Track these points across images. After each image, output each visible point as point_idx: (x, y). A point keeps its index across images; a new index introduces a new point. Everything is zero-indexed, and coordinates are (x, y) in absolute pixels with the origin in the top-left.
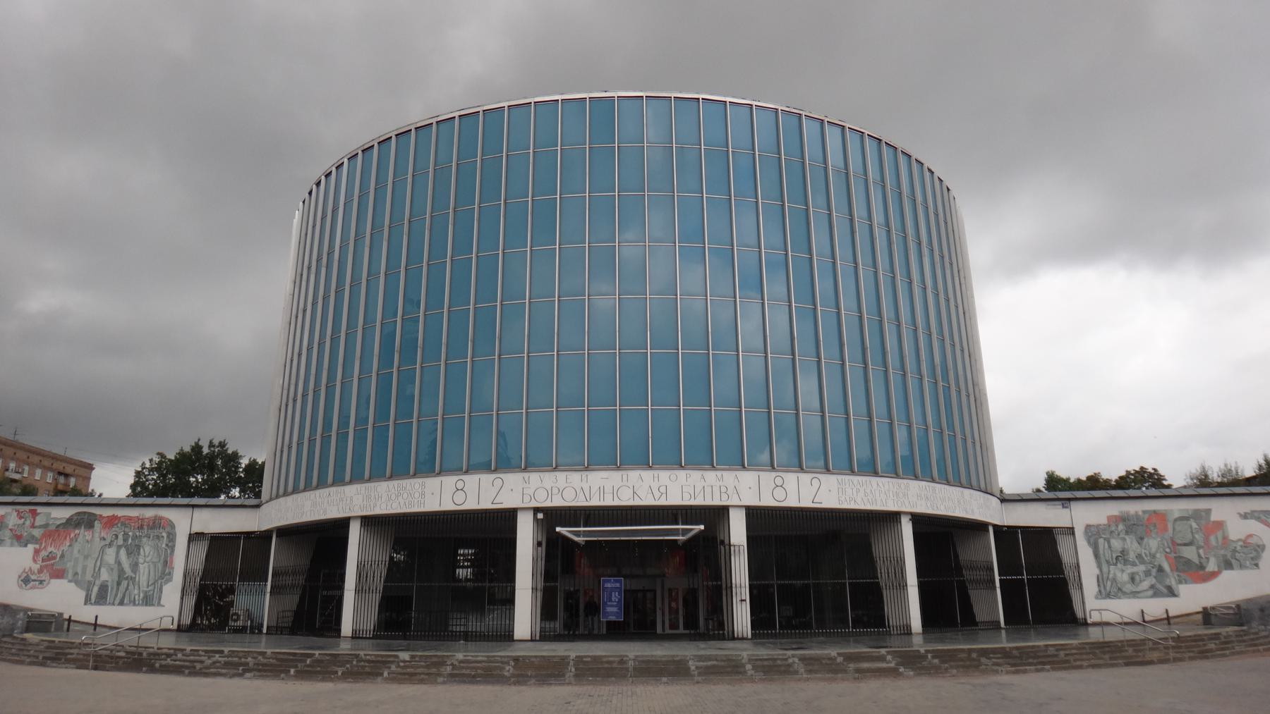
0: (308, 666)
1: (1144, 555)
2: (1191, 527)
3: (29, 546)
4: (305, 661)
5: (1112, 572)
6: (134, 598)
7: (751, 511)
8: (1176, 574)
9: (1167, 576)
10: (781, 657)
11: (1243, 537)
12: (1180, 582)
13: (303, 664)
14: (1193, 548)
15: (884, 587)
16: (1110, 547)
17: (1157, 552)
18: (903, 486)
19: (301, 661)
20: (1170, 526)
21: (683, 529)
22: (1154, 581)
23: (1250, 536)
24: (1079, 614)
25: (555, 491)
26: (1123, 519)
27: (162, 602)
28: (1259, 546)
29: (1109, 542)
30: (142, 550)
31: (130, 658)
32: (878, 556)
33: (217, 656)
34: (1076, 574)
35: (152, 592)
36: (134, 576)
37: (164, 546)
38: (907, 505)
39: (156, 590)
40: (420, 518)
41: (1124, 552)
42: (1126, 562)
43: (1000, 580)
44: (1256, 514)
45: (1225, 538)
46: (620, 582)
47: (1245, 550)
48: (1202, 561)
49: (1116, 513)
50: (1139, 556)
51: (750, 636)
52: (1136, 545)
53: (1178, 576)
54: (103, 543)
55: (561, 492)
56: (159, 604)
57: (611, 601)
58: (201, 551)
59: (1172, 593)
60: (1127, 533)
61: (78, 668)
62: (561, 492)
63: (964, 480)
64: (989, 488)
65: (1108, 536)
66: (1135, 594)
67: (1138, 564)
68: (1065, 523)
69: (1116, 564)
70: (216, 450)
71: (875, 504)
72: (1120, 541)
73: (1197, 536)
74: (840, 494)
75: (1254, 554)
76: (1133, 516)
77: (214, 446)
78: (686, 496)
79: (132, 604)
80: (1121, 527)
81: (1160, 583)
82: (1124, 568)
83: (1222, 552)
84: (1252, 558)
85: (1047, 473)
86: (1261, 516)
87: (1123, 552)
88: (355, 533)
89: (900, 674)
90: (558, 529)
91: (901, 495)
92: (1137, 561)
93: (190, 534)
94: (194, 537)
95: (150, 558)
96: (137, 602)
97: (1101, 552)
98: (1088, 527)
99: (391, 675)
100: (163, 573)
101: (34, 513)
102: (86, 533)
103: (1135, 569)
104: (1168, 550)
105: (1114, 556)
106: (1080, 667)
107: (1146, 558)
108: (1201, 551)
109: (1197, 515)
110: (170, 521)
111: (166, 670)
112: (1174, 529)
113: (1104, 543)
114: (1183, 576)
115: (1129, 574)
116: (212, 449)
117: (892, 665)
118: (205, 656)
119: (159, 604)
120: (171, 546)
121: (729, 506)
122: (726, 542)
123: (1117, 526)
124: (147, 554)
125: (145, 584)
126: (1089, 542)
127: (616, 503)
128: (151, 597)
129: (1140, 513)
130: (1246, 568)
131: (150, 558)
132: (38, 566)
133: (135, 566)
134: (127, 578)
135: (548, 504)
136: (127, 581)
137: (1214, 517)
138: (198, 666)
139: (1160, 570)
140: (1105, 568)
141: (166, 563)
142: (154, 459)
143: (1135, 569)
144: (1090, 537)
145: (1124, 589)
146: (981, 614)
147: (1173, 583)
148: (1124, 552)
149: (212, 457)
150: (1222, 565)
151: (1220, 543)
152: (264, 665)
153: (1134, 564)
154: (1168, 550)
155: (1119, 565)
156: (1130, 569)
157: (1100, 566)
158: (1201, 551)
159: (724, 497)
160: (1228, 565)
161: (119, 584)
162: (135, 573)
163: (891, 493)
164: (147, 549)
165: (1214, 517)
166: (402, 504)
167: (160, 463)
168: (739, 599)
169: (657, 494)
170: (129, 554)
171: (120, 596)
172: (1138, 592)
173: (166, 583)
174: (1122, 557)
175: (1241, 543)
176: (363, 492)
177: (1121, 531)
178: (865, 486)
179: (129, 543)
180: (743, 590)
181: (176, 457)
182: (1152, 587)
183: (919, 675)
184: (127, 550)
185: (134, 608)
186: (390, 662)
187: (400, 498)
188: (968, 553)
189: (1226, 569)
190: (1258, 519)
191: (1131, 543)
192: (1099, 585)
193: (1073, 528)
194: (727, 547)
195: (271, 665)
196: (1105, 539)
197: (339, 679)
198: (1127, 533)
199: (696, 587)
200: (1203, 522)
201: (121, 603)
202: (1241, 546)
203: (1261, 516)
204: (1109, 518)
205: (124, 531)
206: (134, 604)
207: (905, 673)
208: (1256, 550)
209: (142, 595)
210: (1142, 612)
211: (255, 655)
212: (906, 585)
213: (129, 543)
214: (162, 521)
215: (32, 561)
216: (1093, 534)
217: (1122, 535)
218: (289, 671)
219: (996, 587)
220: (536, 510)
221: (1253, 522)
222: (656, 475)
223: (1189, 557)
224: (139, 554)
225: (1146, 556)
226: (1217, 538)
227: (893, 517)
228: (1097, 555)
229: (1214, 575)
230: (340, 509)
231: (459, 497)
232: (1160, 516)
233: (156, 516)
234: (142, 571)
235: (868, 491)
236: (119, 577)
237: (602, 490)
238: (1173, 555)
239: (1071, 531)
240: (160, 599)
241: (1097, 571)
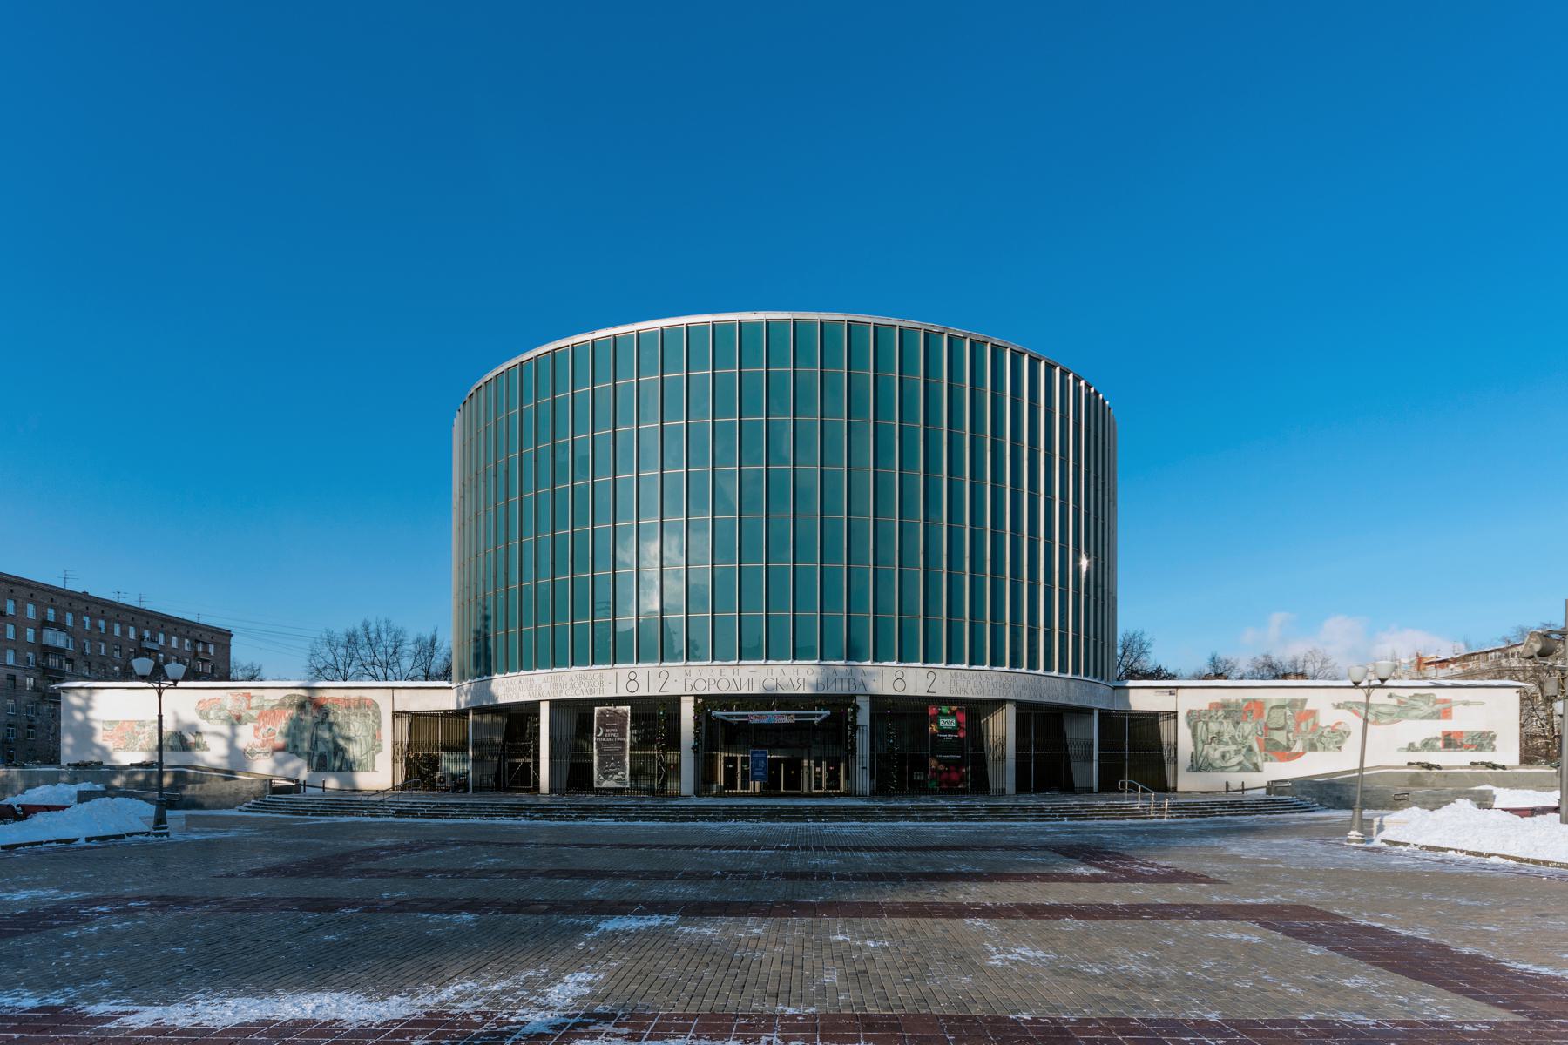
1: (1237, 737)
2: (1285, 714)
3: (249, 724)
8: (1263, 753)
9: (1255, 755)
11: (1332, 724)
12: (1266, 760)
14: (1283, 733)
16: (1207, 729)
17: (1249, 734)
20: (1266, 712)
22: (1242, 758)
23: (1339, 723)
24: (1171, 784)
25: (712, 682)
27: (376, 769)
28: (1345, 732)
29: (1207, 725)
30: (351, 726)
37: (371, 722)
38: (1012, 693)
42: (1220, 742)
43: (1099, 755)
44: (1349, 705)
45: (1315, 725)
47: (1331, 735)
48: (1290, 743)
50: (1233, 738)
51: (868, 794)
52: (1231, 727)
53: (1266, 755)
54: (316, 721)
55: (717, 683)
56: (373, 770)
57: (758, 767)
58: (404, 725)
59: (1257, 769)
60: (1225, 717)
62: (717, 683)
65: (1207, 719)
67: (1230, 743)
69: (1210, 744)
72: (1217, 724)
73: (1289, 722)
75: (1339, 738)
80: (1221, 712)
81: (1248, 760)
82: (1217, 747)
83: (1310, 736)
84: (1336, 742)
86: (1354, 706)
87: (1218, 733)
91: (1007, 686)
94: (396, 715)
98: (1190, 712)
101: (249, 697)
103: (1227, 748)
104: (1260, 733)
105: (1210, 737)
108: (1290, 735)
109: (1293, 704)
112: (1269, 715)
114: (1270, 755)
119: (373, 770)
126: (1189, 724)
129: (1241, 701)
130: (1329, 749)
132: (261, 741)
135: (706, 692)
137: (1308, 707)
139: (1250, 749)
140: (1200, 748)
141: (374, 736)
143: (1227, 748)
145: (1214, 765)
146: (1078, 781)
147: (1259, 760)
148: (1219, 734)
150: (1308, 747)
151: (1310, 728)
153: (1227, 744)
154: (1260, 733)
155: (1213, 744)
156: (1222, 748)
158: (1290, 735)
160: (1313, 747)
165: (1308, 707)
166: (584, 689)
168: (861, 766)
169: (796, 685)
172: (1227, 767)
173: (377, 753)
175: (1329, 729)
176: (550, 680)
180: (865, 760)
182: (1240, 763)
187: (582, 686)
188: (1074, 732)
189: (1310, 750)
190: (1350, 709)
196: (1204, 722)
198: (1225, 717)
199: (838, 755)
200: (1297, 710)
202: (1329, 732)
203: (1354, 706)
208: (1341, 735)
210: (1227, 783)
215: (253, 737)
216: (1194, 718)
217: (1220, 720)
220: (697, 697)
221: (1345, 711)
222: (796, 670)
223: (1278, 740)
224: (349, 730)
225: (1239, 737)
226: (1307, 725)
228: (1194, 736)
229: (1298, 755)
230: (531, 694)
231: (633, 686)
232: (1258, 705)
233: (360, 698)
238: (1263, 738)
239: (1174, 715)
240: (374, 766)
241: (1192, 749)
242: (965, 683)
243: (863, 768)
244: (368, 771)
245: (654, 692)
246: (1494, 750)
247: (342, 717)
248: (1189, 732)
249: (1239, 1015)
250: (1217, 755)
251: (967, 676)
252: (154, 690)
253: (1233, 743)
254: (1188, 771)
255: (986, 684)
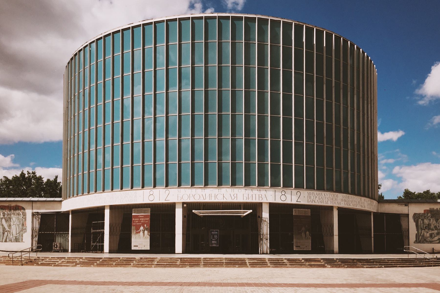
0: (101, 262)
4: (99, 261)
5: (423, 233)
6: (11, 239)
7: (271, 205)
10: (280, 259)
13: (99, 262)
15: (324, 235)
16: (423, 222)
18: (335, 196)
19: (98, 260)
21: (243, 212)
25: (191, 196)
26: (431, 211)
27: (23, 241)
30: (12, 219)
31: (27, 261)
32: (322, 223)
33: (63, 259)
34: (407, 233)
35: (18, 237)
36: (10, 230)
37: (21, 218)
39: (20, 236)
40: (127, 206)
41: (429, 225)
42: (429, 229)
46: (217, 231)
49: (428, 209)
50: (435, 227)
52: (435, 222)
61: (7, 265)
63: (362, 194)
64: (373, 196)
65: (423, 218)
66: (431, 242)
68: (406, 212)
69: (425, 230)
70: (31, 175)
71: (323, 203)
72: (428, 220)
74: (309, 198)
76: (435, 210)
77: (30, 174)
78: (245, 198)
79: (10, 242)
85: (405, 190)
88: (107, 212)
89: (326, 267)
90: (193, 211)
91: (334, 199)
92: (434, 229)
93: (32, 213)
94: (33, 215)
95: (16, 223)
96: (12, 241)
97: (419, 224)
98: (415, 214)
99: (134, 265)
100: (22, 229)
102: (3, 211)
103: (433, 232)
105: (425, 226)
106: (396, 267)
107: (438, 228)
110: (23, 207)
111: (42, 264)
113: (421, 221)
115: (430, 234)
116: (29, 175)
117: (323, 264)
118: (58, 259)
120: (24, 218)
121: (104, 206)
122: (261, 217)
123: (428, 214)
124: (14, 221)
125: (15, 233)
127: (216, 201)
128: (18, 239)
131: (16, 223)
133: (10, 226)
134: (7, 231)
136: (7, 232)
138: (57, 263)
140: (420, 231)
141: (23, 225)
142: (3, 179)
143: (433, 232)
144: (415, 218)
145: (427, 240)
148: (429, 225)
149: (29, 179)
152: (83, 262)
153: (433, 230)
156: (431, 232)
157: (418, 230)
159: (261, 199)
161: (3, 234)
162: (10, 229)
163: (330, 198)
164: (14, 218)
167: (6, 181)
169: (233, 197)
170: (6, 221)
171: (5, 238)
172: (433, 241)
173: (24, 233)
174: (428, 227)
177: (429, 216)
178: (319, 196)
179: (6, 217)
181: (12, 178)
183: (333, 267)
184: (5, 220)
185: (12, 243)
186: (132, 260)
191: (433, 221)
192: (416, 238)
193: (408, 214)
194: (261, 219)
195: (86, 262)
197: (114, 266)
198: (432, 217)
201: (6, 241)
204: (425, 211)
205: (3, 212)
206: (11, 242)
207: (327, 266)
209: (14, 238)
210: (433, 248)
211: (78, 259)
212: (333, 235)
213: (6, 217)
214: (19, 207)
216: (417, 217)
218: (94, 264)
219: (372, 237)
220: (183, 203)
224: (11, 221)
227: (331, 208)
228: (417, 226)
233: (16, 205)
234: (13, 228)
235: (320, 197)
236: (3, 231)
237: (210, 196)
240: (22, 239)
241: (416, 232)
242: (315, 197)
243: (266, 239)
244: (19, 242)
245: (164, 201)
246: (429, 190)
247: (7, 215)
248: (414, 224)
249: (239, 282)
250: (428, 235)
251: (315, 194)
252: (30, 246)
253: (436, 230)
254: (414, 243)
255: (324, 198)
